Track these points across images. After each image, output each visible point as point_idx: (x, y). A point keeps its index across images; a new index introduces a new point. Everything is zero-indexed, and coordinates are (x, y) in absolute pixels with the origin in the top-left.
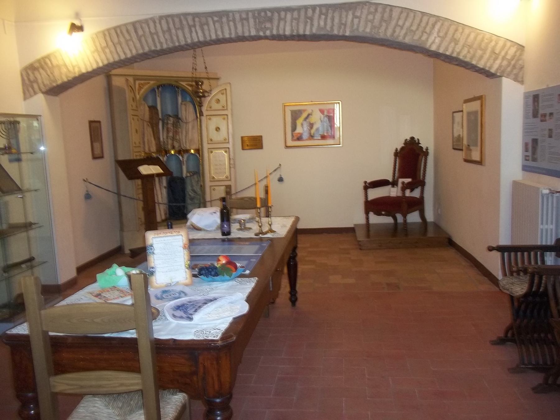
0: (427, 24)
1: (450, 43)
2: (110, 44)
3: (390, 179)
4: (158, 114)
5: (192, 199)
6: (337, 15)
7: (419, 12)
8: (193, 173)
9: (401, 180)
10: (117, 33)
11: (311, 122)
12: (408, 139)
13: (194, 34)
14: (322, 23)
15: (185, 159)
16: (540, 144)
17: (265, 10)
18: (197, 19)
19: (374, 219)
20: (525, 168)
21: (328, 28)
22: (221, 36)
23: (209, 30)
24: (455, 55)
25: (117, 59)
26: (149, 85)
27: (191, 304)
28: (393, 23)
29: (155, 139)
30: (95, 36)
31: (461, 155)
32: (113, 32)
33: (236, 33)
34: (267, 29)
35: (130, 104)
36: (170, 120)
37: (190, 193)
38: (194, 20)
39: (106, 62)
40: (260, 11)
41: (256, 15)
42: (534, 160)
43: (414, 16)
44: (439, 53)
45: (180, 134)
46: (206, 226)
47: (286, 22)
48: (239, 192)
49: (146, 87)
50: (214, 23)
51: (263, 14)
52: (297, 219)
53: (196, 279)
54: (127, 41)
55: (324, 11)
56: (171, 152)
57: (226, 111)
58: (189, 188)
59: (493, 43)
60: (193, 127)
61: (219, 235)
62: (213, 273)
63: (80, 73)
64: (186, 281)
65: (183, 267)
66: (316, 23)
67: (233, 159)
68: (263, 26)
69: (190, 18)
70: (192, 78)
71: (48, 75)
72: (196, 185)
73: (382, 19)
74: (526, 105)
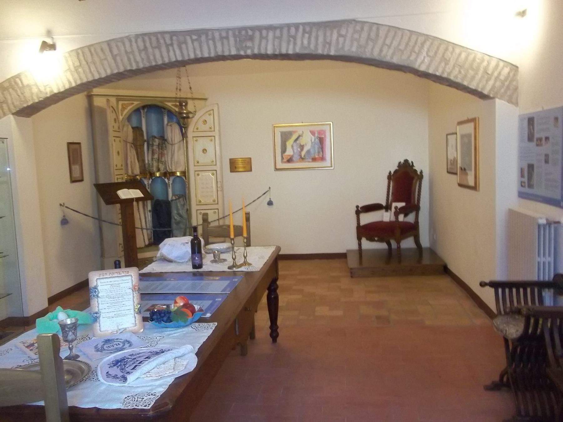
0: (416, 43)
1: (440, 63)
2: (84, 63)
3: (384, 204)
4: (142, 135)
5: (178, 223)
6: (321, 34)
7: (408, 32)
8: (178, 197)
9: (394, 205)
10: (90, 52)
11: (302, 144)
12: (402, 161)
13: (172, 53)
14: (306, 42)
15: (171, 182)
16: (536, 170)
17: (245, 29)
18: (174, 38)
19: (367, 245)
20: (522, 195)
21: (312, 46)
22: (199, 56)
23: (187, 49)
24: (445, 75)
25: (91, 79)
26: (133, 106)
27: (133, 357)
28: (380, 42)
29: (138, 161)
30: (67, 55)
31: (455, 180)
32: (87, 50)
33: (216, 52)
34: (249, 48)
35: (111, 125)
36: (155, 142)
37: (176, 217)
38: (171, 39)
39: (79, 82)
40: (240, 29)
41: (237, 33)
42: (530, 186)
43: (402, 35)
44: (429, 73)
45: (166, 156)
46: (177, 257)
47: (267, 41)
48: (226, 216)
49: (129, 108)
50: (193, 41)
51: (243, 32)
52: (278, 249)
53: (149, 324)
54: (101, 60)
55: (308, 29)
56: (177, 174)
57: (214, 132)
58: (174, 212)
59: (485, 64)
60: (179, 149)
61: (189, 268)
62: (165, 319)
63: (52, 94)
64: (135, 327)
65: (132, 312)
66: (299, 42)
67: (220, 182)
68: (244, 45)
69: (167, 37)
70: (176, 98)
71: (19, 96)
72: (182, 209)
73: (369, 38)
74: (521, 128)
